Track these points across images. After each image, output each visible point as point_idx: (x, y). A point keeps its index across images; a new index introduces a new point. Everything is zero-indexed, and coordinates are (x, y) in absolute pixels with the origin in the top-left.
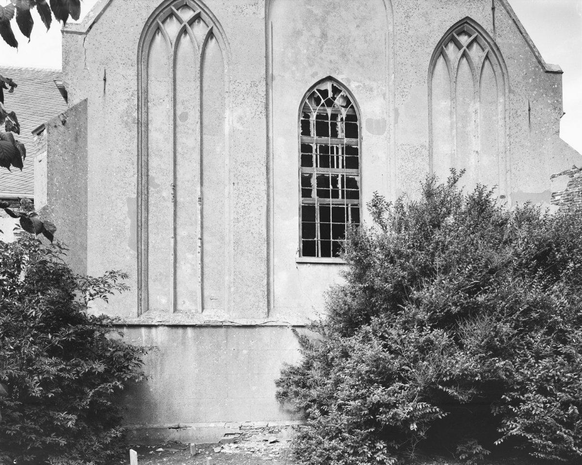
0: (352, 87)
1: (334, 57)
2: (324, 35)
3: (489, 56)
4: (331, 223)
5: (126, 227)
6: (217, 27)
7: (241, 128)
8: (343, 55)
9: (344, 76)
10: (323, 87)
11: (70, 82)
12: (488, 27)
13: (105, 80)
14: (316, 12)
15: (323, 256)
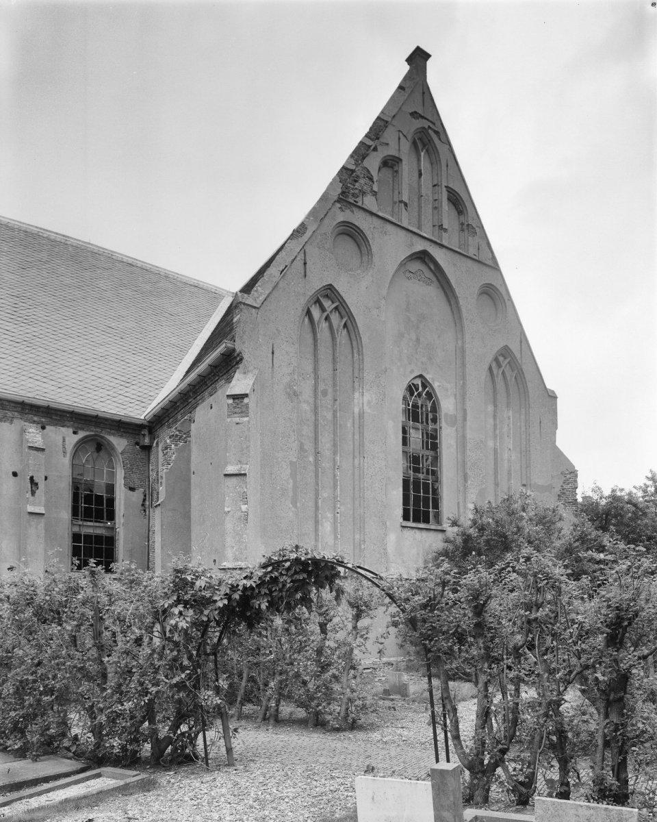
0: (436, 385)
1: (424, 359)
2: (418, 340)
3: (347, 324)
4: (422, 494)
5: (289, 486)
6: (351, 322)
7: (369, 411)
8: (430, 359)
9: (431, 376)
10: (416, 382)
11: (246, 350)
12: (518, 355)
13: (273, 353)
14: (413, 319)
15: (414, 521)
